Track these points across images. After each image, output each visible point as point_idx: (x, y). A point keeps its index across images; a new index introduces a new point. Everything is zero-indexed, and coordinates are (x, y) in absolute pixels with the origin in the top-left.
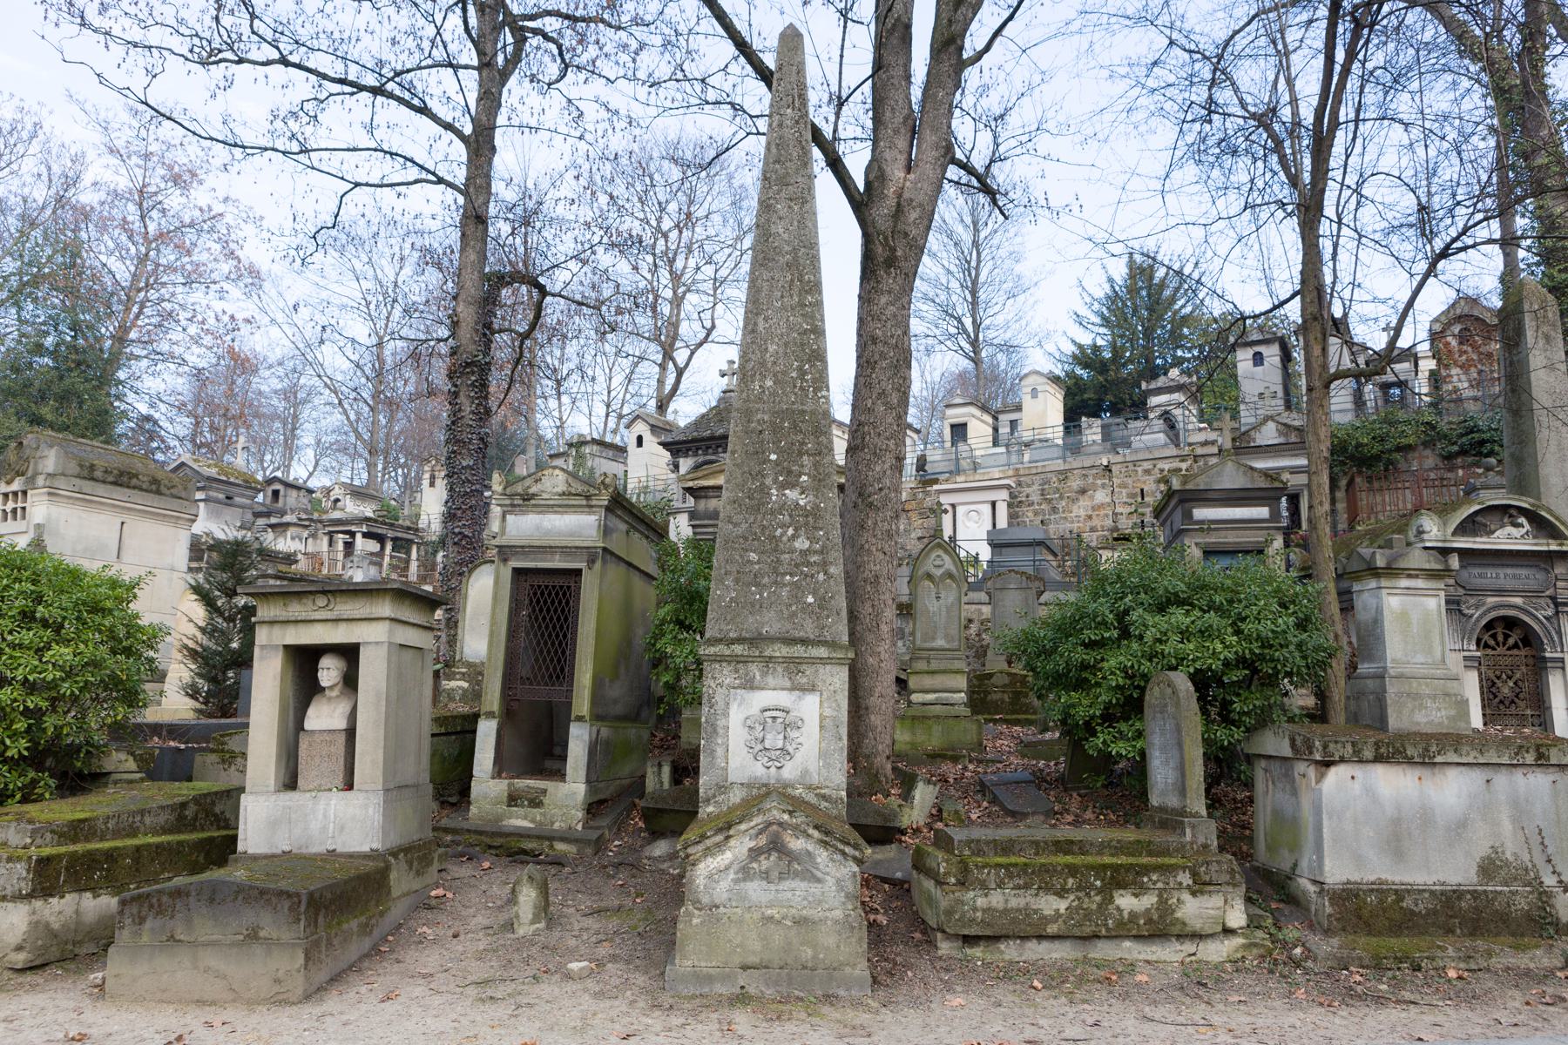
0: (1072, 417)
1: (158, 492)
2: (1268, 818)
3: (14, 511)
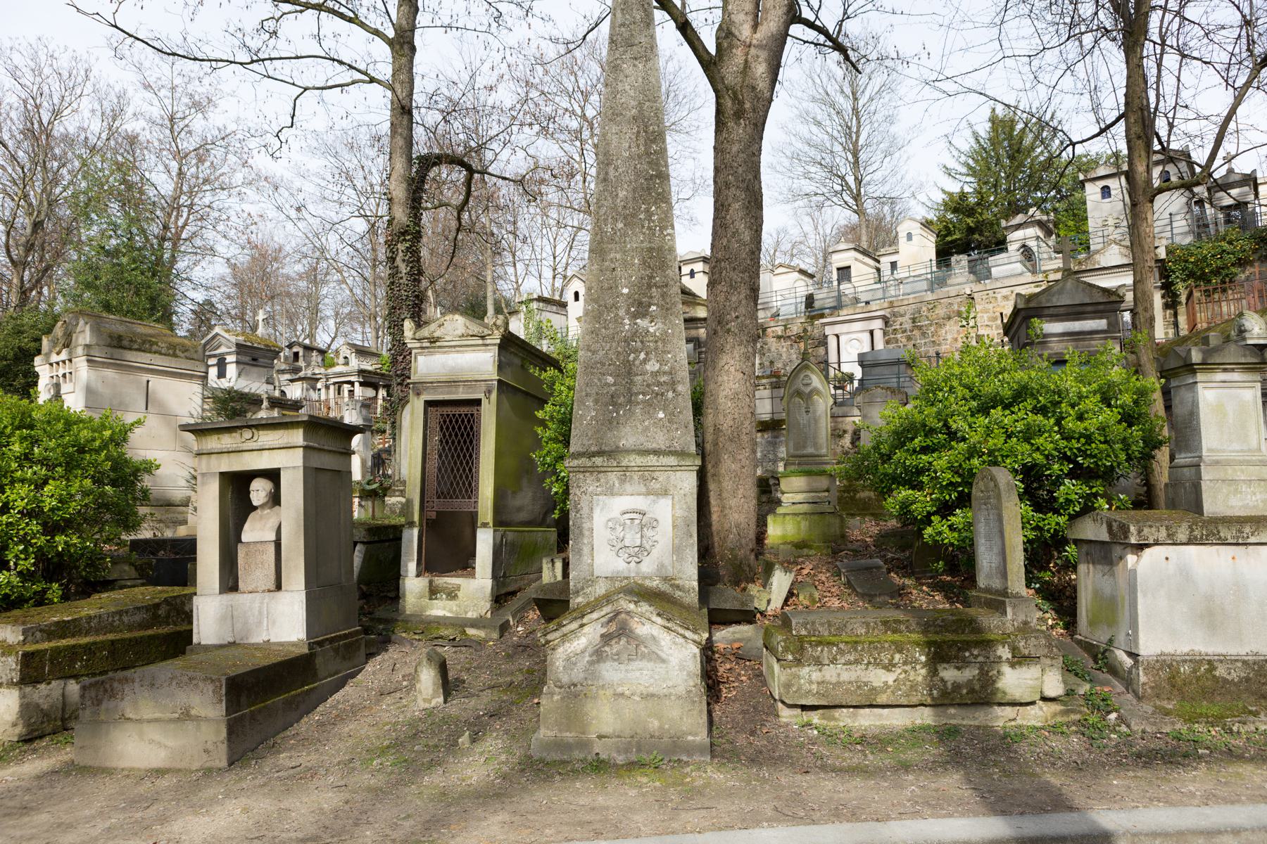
0: (944, 254)
1: (175, 355)
2: (1089, 597)
3: (64, 376)
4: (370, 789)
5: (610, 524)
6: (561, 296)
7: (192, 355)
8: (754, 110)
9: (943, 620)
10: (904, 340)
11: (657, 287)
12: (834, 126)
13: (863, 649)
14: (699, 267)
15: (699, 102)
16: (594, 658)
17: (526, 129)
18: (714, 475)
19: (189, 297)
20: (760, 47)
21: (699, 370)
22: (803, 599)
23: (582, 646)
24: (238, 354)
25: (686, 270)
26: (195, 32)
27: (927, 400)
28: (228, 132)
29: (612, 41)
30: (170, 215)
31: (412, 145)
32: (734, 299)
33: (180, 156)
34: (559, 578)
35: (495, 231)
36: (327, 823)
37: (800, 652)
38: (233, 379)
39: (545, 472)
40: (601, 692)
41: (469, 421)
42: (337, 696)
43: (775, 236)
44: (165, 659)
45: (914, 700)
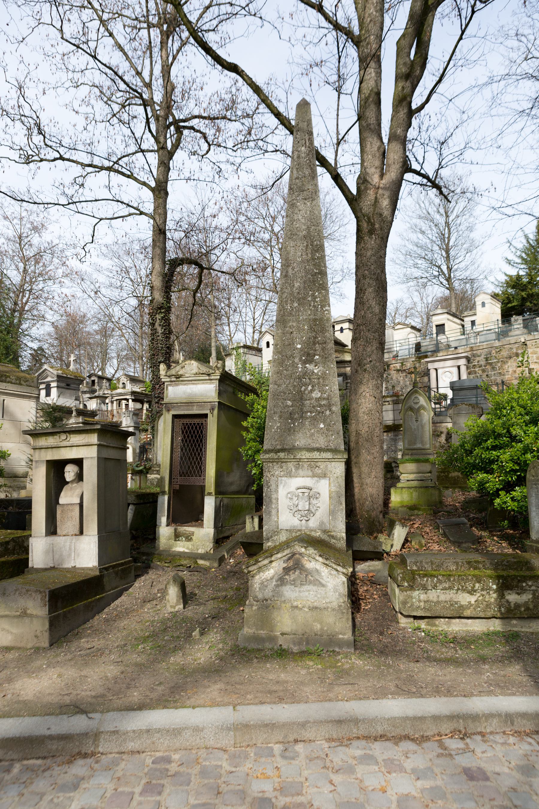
1: (20, 384)
4: (137, 665)
5: (289, 496)
6: (258, 344)
7: (29, 383)
8: (381, 229)
9: (508, 562)
10: (480, 372)
11: (319, 344)
12: (433, 234)
13: (454, 580)
14: (346, 325)
15: (346, 221)
16: (279, 583)
17: (237, 241)
18: (356, 463)
19: (29, 345)
20: (384, 188)
21: (346, 394)
22: (414, 544)
23: (271, 575)
24: (58, 381)
25: (338, 327)
26: (35, 186)
27: (496, 415)
28: (54, 244)
29: (290, 189)
30: (18, 296)
31: (165, 252)
32: (369, 349)
33: (25, 260)
34: (257, 528)
35: (217, 303)
36: (110, 686)
37: (412, 581)
38: (54, 398)
39: (247, 460)
40: (283, 605)
41: (200, 428)
42: (117, 602)
43: (395, 304)
44: (11, 577)
45: (489, 614)
